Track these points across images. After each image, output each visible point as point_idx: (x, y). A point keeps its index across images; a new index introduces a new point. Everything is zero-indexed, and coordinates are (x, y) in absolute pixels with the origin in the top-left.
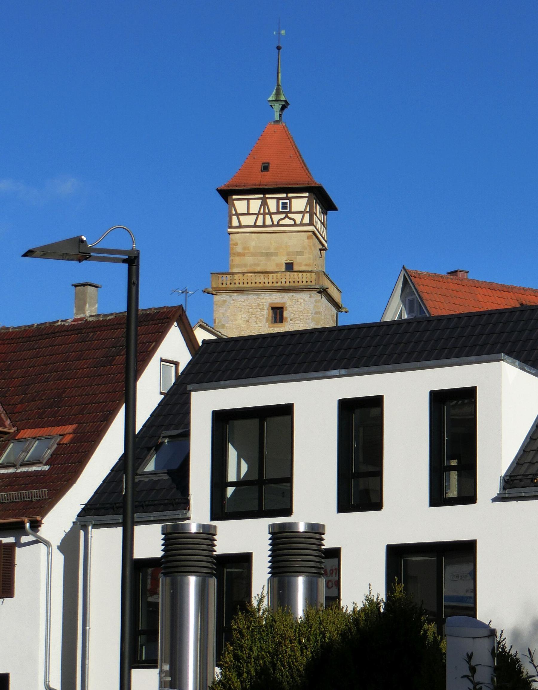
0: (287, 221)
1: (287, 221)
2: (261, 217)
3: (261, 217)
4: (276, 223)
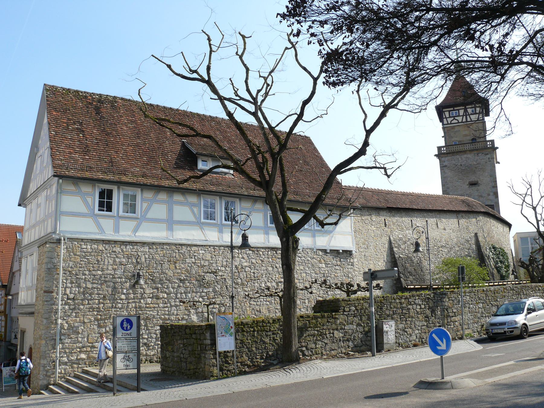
0: (455, 121)
1: (455, 121)
2: (464, 117)
3: (464, 117)
4: (449, 123)
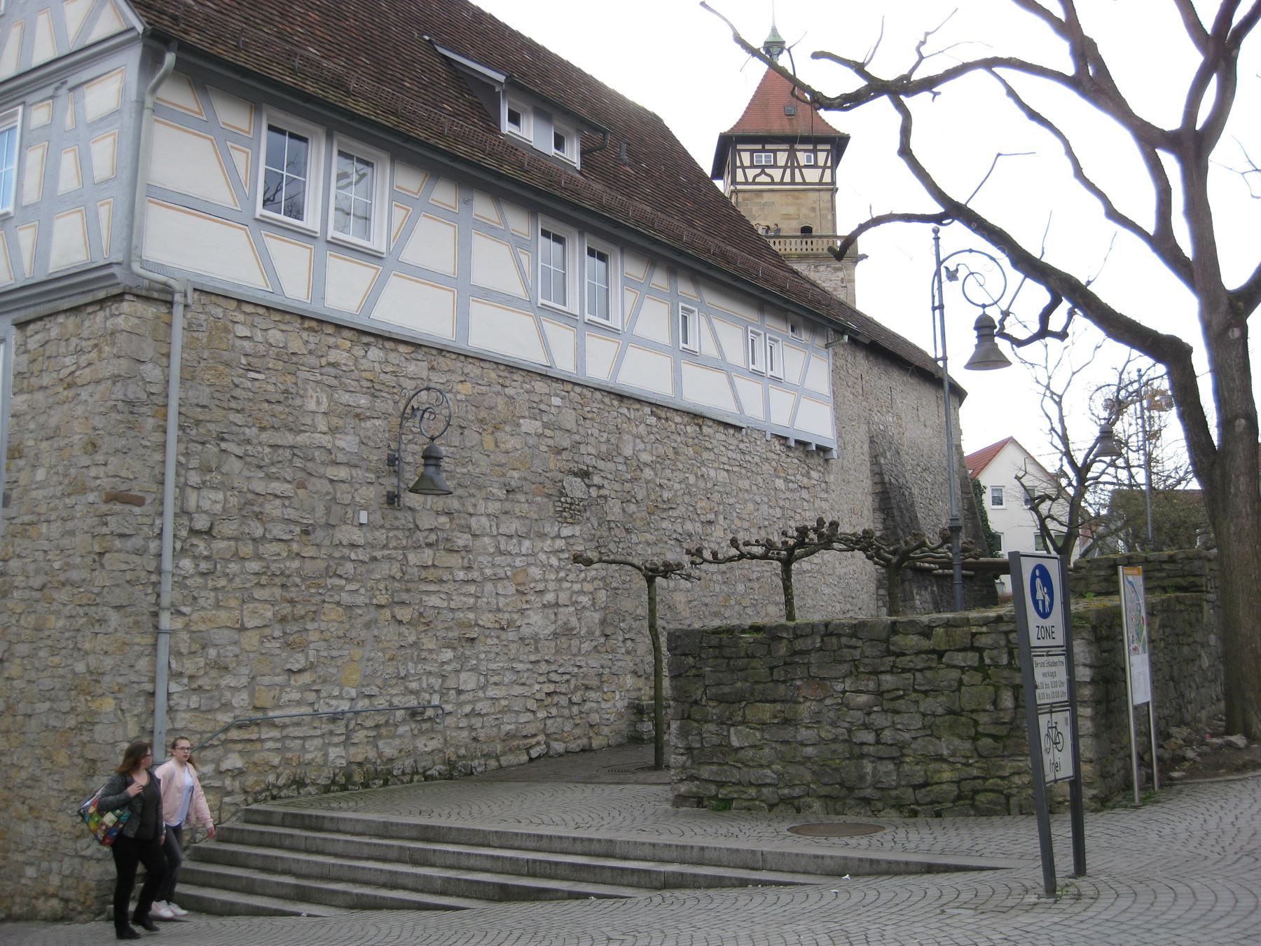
0: (763, 178)
1: (763, 178)
2: (788, 171)
3: (788, 171)
4: (750, 180)
